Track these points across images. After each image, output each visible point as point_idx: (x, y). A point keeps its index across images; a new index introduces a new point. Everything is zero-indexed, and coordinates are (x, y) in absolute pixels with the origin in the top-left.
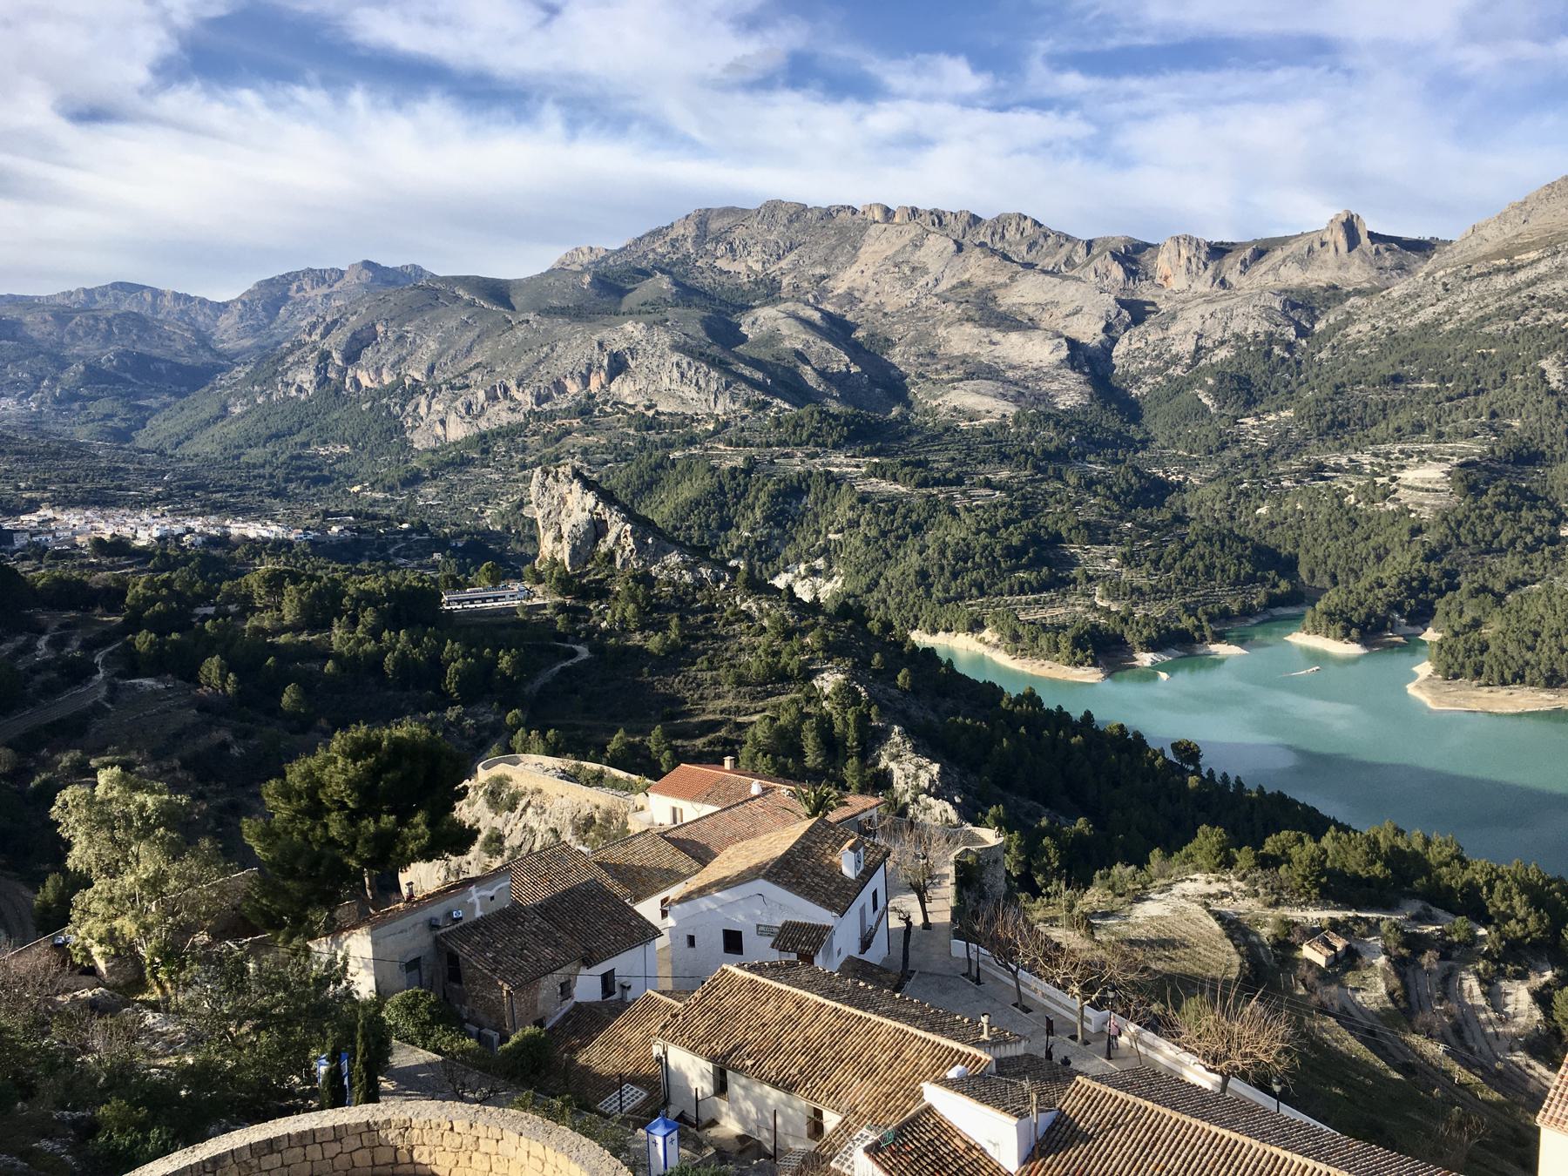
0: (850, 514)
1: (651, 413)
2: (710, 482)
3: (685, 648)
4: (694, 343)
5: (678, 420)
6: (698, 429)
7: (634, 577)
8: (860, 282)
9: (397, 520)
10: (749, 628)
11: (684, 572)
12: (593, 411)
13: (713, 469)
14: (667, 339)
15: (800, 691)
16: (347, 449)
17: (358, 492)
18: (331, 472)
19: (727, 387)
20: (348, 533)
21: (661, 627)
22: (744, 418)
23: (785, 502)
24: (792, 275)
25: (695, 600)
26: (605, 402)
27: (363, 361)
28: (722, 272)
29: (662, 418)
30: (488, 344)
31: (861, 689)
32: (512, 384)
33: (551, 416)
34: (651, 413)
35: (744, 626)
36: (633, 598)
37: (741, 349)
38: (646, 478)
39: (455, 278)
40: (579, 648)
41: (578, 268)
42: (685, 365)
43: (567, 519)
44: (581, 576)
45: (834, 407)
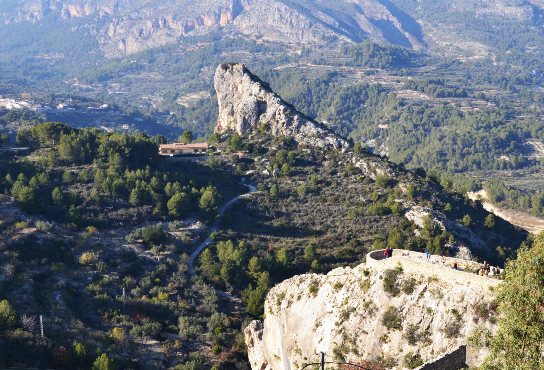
2: (303, 88)
16: (62, 56)
22: (321, 47)
26: (230, 33)
32: (169, 18)
42: (283, 10)
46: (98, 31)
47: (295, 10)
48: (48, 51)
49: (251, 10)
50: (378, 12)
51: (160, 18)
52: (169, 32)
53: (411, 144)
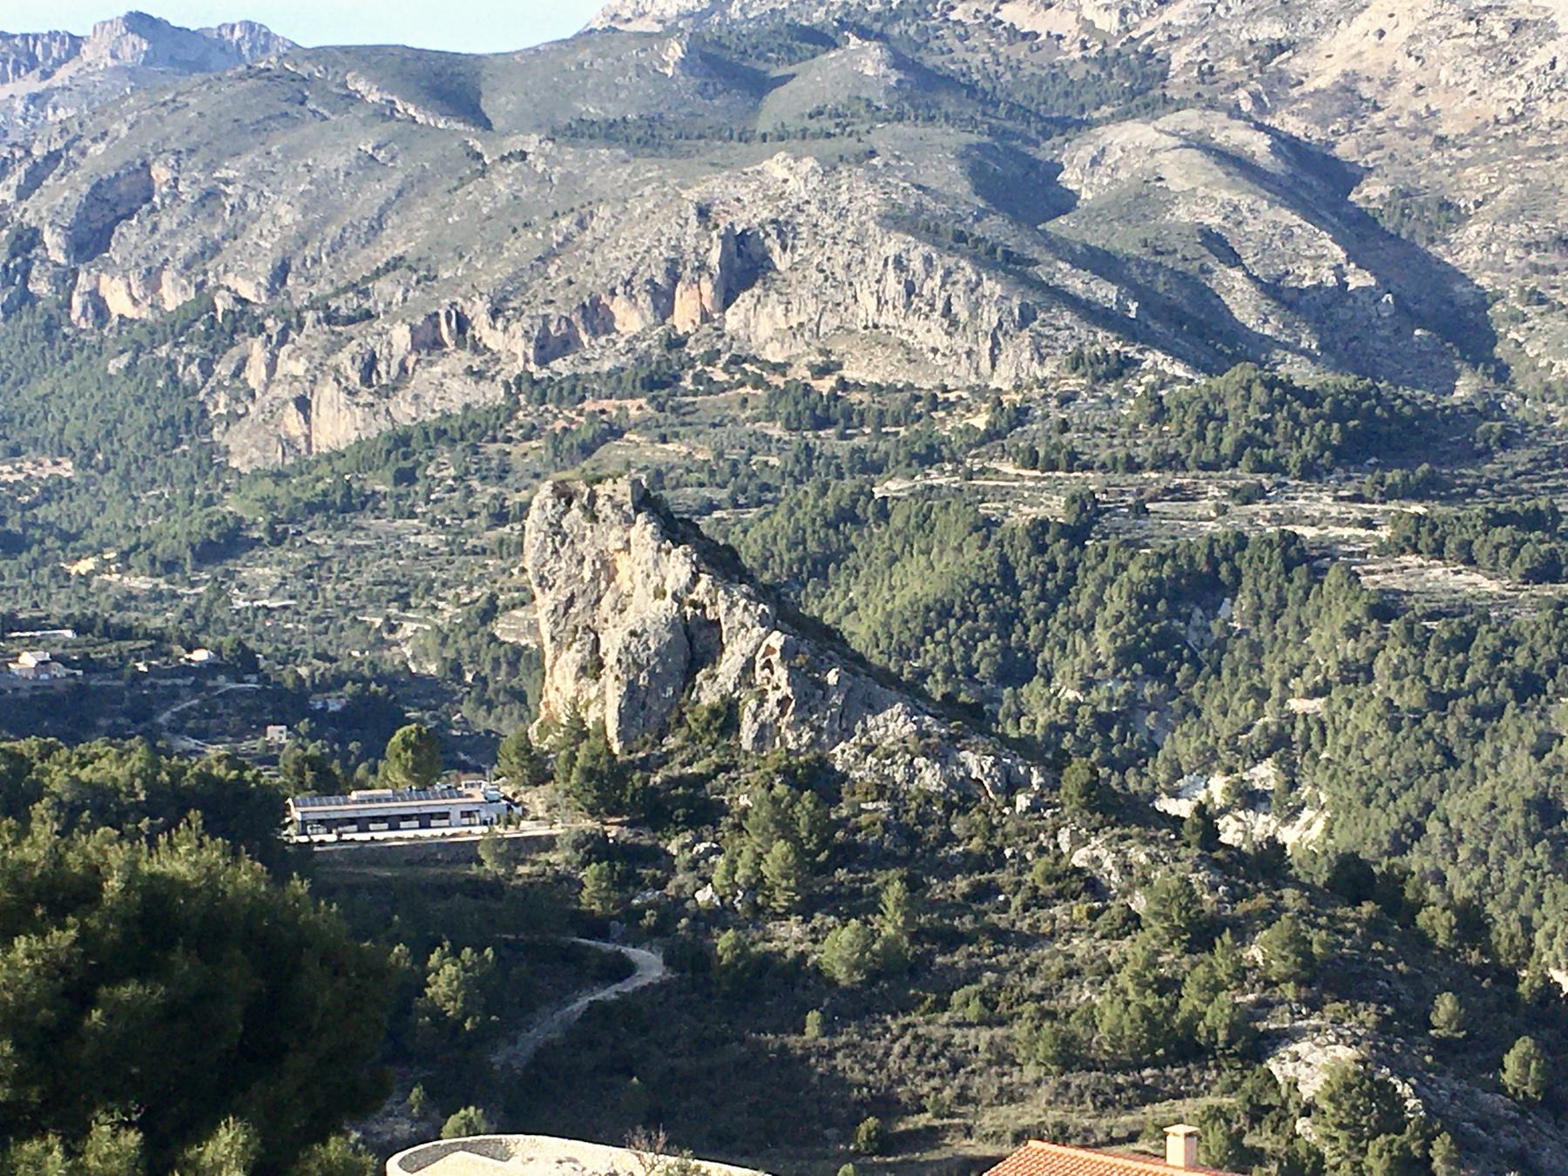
0: (1348, 648)
1: (826, 385)
2: (974, 558)
3: (923, 962)
4: (942, 209)
5: (895, 403)
6: (947, 426)
7: (788, 773)
8: (1374, 59)
9: (181, 640)
10: (1093, 915)
11: (920, 762)
12: (678, 378)
13: (986, 526)
14: (872, 199)
15: (1233, 1088)
16: (67, 468)
17: (91, 573)
18: (25, 526)
19: (1026, 317)
20: (59, 670)
21: (860, 904)
22: (1066, 399)
23: (1173, 614)
24: (1196, 43)
25: (948, 838)
26: (711, 357)
27: (115, 254)
28: (1015, 35)
29: (855, 397)
30: (425, 210)
31: (1404, 1089)
32: (478, 311)
33: (574, 390)
34: (826, 385)
35: (1079, 909)
36: (785, 827)
37: (1061, 225)
38: (812, 546)
39: (346, 50)
40: (637, 954)
41: (646, 26)
42: (917, 265)
43: (614, 618)
44: (646, 765)
45: (1302, 373)
46: (207, 371)
47: (963, 263)
48: (16, 452)
49: (793, 269)
50: (1297, 256)
51: (442, 313)
52: (477, 363)
53: (1417, 770)
